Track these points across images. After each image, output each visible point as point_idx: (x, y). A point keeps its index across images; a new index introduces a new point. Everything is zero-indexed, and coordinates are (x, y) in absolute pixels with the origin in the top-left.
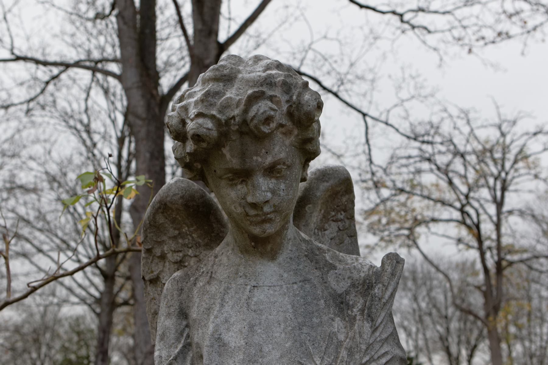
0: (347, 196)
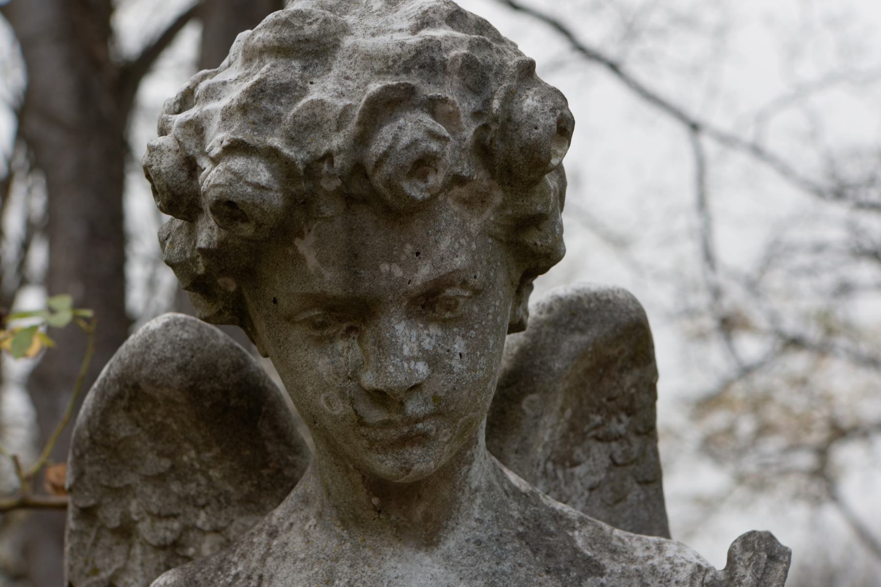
0: (637, 372)
